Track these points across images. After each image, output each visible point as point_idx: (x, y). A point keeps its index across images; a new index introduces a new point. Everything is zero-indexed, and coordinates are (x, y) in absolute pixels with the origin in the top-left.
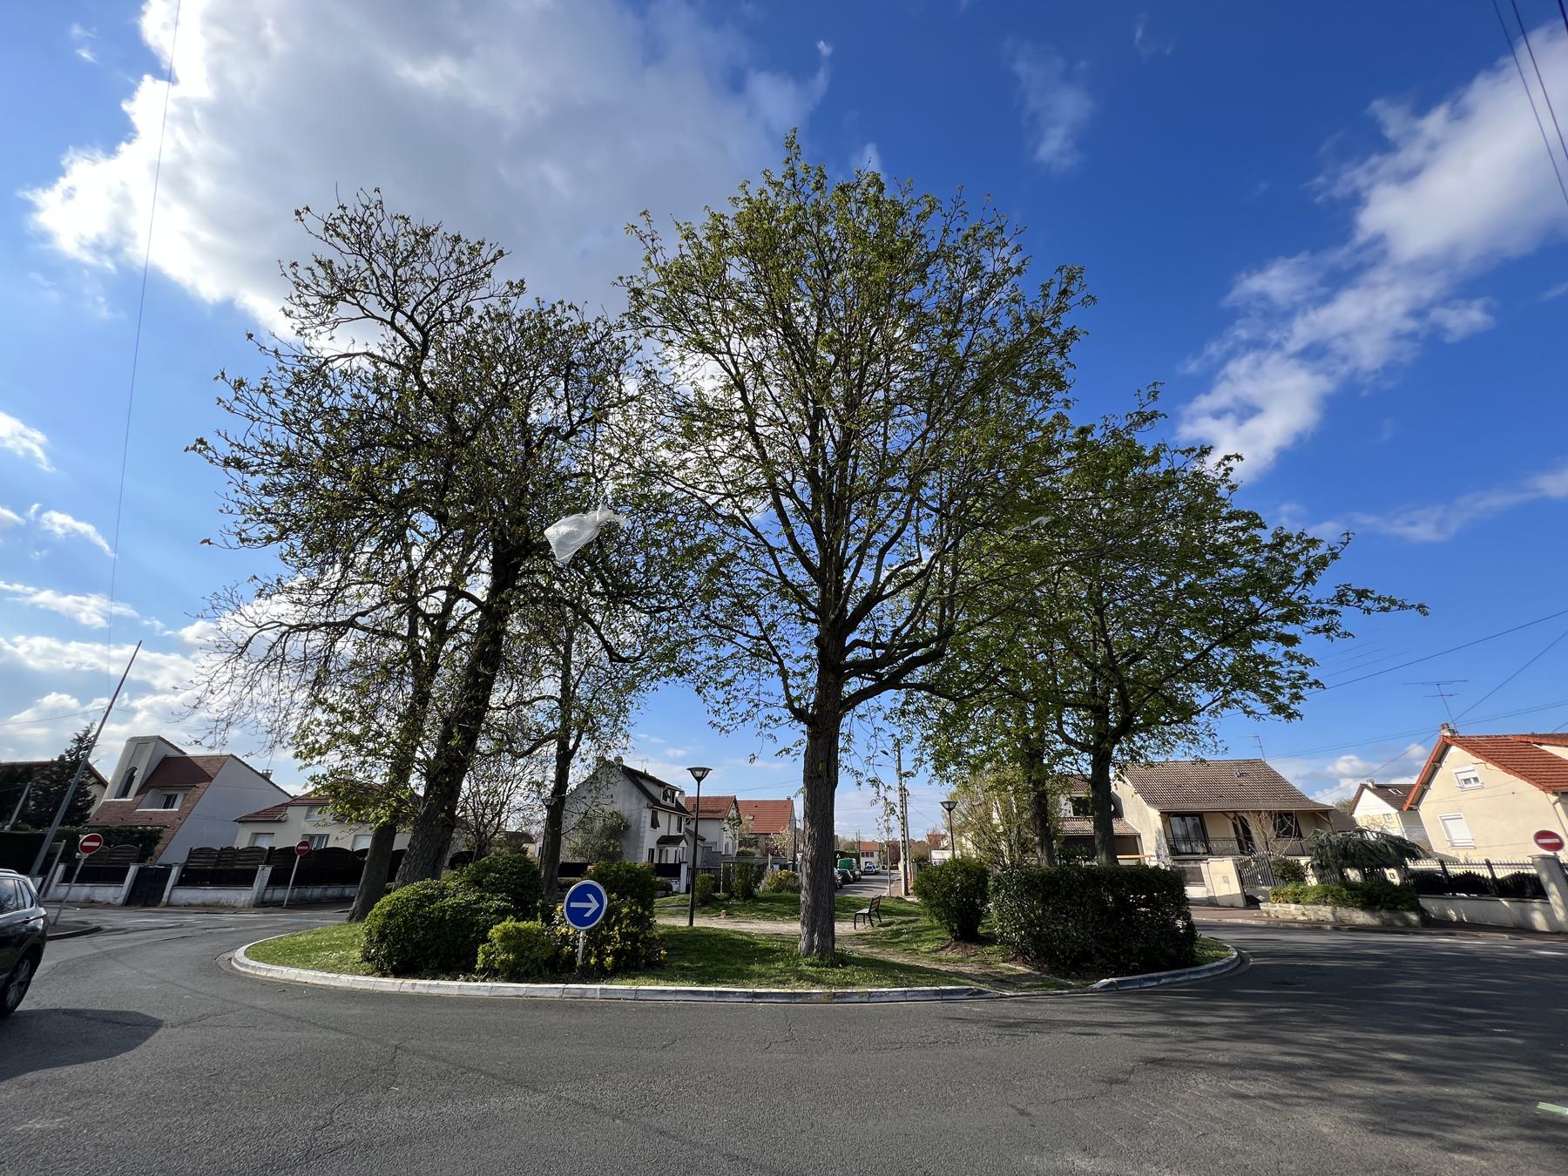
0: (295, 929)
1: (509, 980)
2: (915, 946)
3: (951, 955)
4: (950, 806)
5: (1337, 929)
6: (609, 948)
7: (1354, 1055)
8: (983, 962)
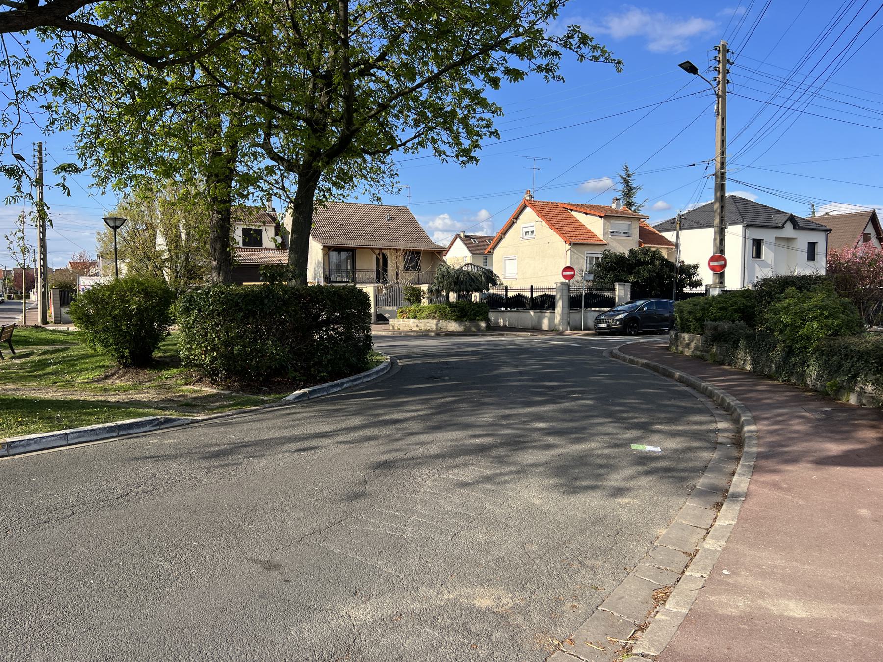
2: (68, 377)
3: (119, 383)
4: (114, 223)
5: (438, 335)
7: (518, 429)
8: (161, 387)
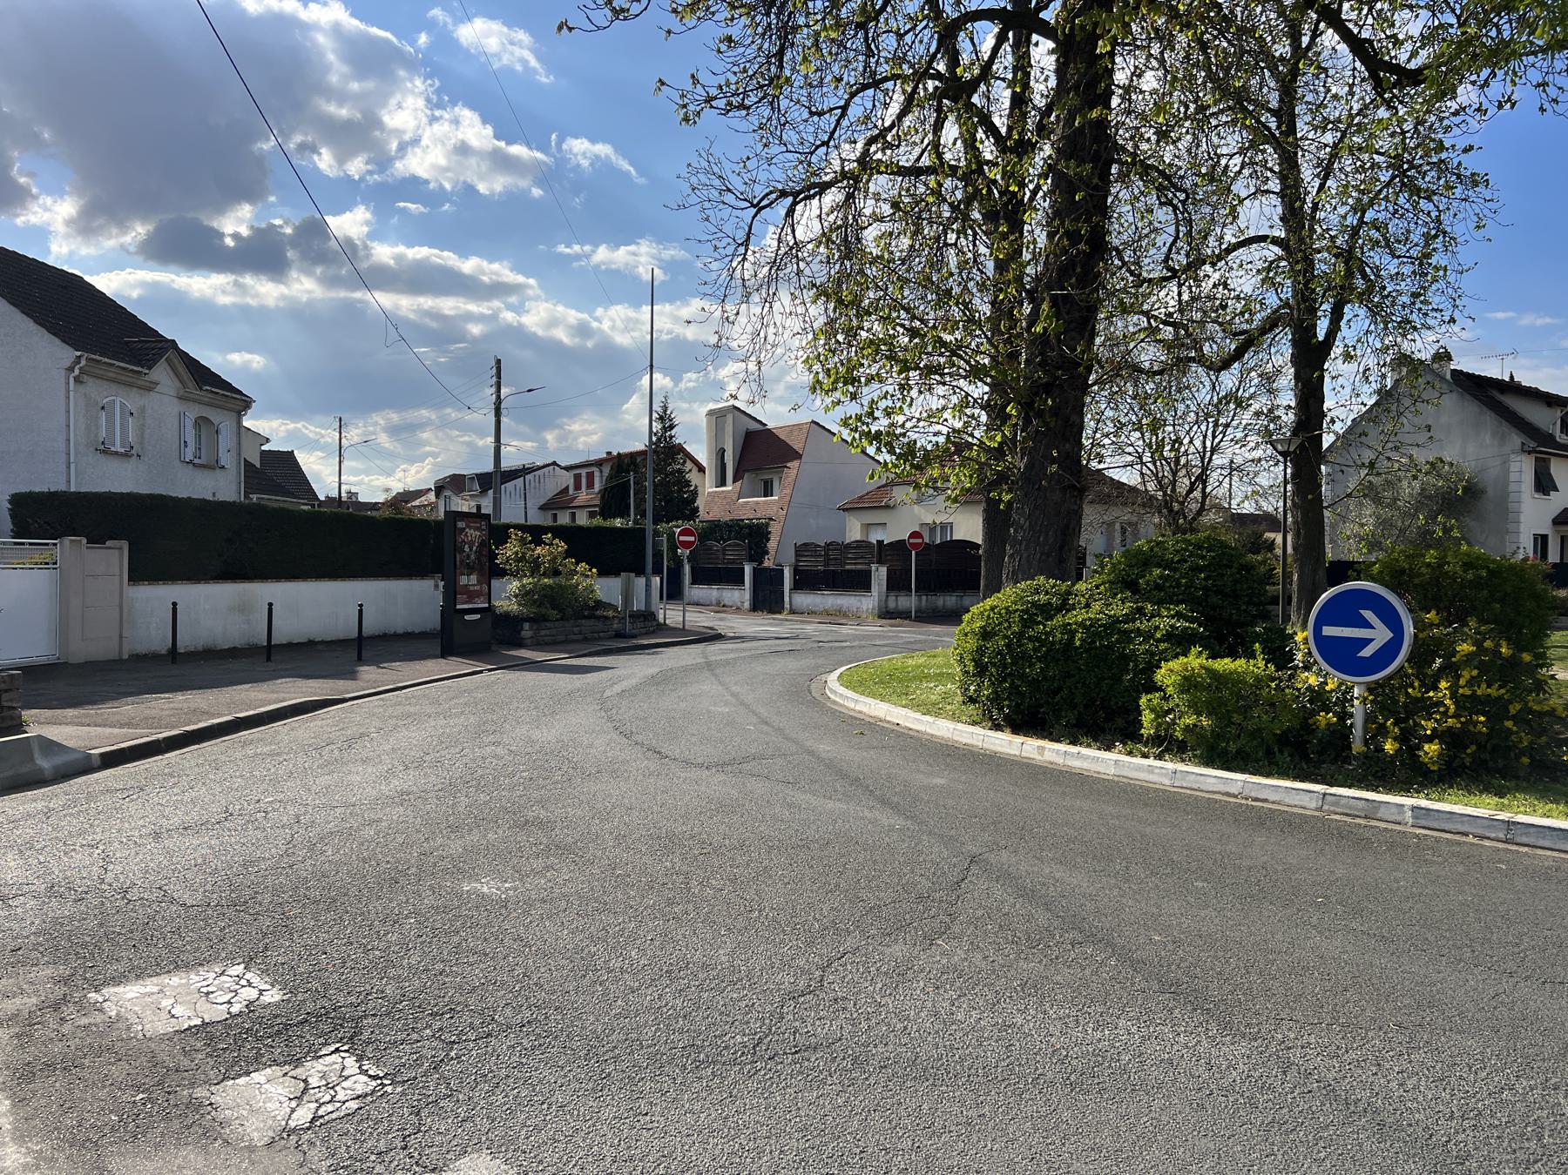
0: (910, 648)
1: (1209, 762)
6: (1429, 726)
